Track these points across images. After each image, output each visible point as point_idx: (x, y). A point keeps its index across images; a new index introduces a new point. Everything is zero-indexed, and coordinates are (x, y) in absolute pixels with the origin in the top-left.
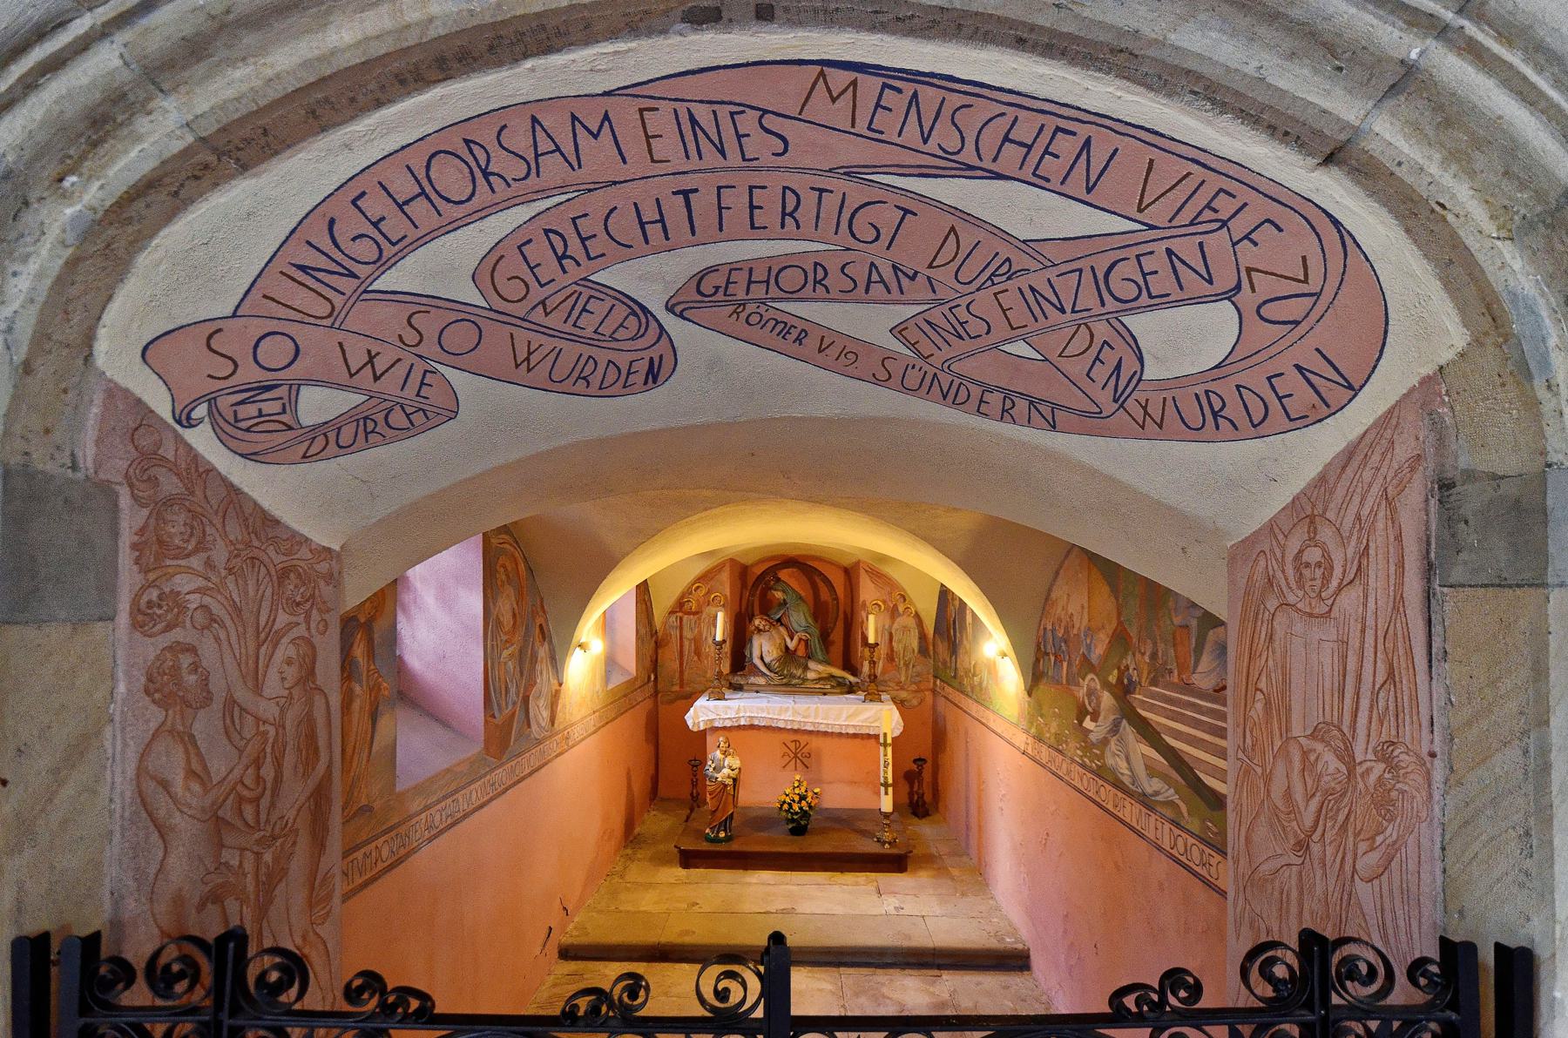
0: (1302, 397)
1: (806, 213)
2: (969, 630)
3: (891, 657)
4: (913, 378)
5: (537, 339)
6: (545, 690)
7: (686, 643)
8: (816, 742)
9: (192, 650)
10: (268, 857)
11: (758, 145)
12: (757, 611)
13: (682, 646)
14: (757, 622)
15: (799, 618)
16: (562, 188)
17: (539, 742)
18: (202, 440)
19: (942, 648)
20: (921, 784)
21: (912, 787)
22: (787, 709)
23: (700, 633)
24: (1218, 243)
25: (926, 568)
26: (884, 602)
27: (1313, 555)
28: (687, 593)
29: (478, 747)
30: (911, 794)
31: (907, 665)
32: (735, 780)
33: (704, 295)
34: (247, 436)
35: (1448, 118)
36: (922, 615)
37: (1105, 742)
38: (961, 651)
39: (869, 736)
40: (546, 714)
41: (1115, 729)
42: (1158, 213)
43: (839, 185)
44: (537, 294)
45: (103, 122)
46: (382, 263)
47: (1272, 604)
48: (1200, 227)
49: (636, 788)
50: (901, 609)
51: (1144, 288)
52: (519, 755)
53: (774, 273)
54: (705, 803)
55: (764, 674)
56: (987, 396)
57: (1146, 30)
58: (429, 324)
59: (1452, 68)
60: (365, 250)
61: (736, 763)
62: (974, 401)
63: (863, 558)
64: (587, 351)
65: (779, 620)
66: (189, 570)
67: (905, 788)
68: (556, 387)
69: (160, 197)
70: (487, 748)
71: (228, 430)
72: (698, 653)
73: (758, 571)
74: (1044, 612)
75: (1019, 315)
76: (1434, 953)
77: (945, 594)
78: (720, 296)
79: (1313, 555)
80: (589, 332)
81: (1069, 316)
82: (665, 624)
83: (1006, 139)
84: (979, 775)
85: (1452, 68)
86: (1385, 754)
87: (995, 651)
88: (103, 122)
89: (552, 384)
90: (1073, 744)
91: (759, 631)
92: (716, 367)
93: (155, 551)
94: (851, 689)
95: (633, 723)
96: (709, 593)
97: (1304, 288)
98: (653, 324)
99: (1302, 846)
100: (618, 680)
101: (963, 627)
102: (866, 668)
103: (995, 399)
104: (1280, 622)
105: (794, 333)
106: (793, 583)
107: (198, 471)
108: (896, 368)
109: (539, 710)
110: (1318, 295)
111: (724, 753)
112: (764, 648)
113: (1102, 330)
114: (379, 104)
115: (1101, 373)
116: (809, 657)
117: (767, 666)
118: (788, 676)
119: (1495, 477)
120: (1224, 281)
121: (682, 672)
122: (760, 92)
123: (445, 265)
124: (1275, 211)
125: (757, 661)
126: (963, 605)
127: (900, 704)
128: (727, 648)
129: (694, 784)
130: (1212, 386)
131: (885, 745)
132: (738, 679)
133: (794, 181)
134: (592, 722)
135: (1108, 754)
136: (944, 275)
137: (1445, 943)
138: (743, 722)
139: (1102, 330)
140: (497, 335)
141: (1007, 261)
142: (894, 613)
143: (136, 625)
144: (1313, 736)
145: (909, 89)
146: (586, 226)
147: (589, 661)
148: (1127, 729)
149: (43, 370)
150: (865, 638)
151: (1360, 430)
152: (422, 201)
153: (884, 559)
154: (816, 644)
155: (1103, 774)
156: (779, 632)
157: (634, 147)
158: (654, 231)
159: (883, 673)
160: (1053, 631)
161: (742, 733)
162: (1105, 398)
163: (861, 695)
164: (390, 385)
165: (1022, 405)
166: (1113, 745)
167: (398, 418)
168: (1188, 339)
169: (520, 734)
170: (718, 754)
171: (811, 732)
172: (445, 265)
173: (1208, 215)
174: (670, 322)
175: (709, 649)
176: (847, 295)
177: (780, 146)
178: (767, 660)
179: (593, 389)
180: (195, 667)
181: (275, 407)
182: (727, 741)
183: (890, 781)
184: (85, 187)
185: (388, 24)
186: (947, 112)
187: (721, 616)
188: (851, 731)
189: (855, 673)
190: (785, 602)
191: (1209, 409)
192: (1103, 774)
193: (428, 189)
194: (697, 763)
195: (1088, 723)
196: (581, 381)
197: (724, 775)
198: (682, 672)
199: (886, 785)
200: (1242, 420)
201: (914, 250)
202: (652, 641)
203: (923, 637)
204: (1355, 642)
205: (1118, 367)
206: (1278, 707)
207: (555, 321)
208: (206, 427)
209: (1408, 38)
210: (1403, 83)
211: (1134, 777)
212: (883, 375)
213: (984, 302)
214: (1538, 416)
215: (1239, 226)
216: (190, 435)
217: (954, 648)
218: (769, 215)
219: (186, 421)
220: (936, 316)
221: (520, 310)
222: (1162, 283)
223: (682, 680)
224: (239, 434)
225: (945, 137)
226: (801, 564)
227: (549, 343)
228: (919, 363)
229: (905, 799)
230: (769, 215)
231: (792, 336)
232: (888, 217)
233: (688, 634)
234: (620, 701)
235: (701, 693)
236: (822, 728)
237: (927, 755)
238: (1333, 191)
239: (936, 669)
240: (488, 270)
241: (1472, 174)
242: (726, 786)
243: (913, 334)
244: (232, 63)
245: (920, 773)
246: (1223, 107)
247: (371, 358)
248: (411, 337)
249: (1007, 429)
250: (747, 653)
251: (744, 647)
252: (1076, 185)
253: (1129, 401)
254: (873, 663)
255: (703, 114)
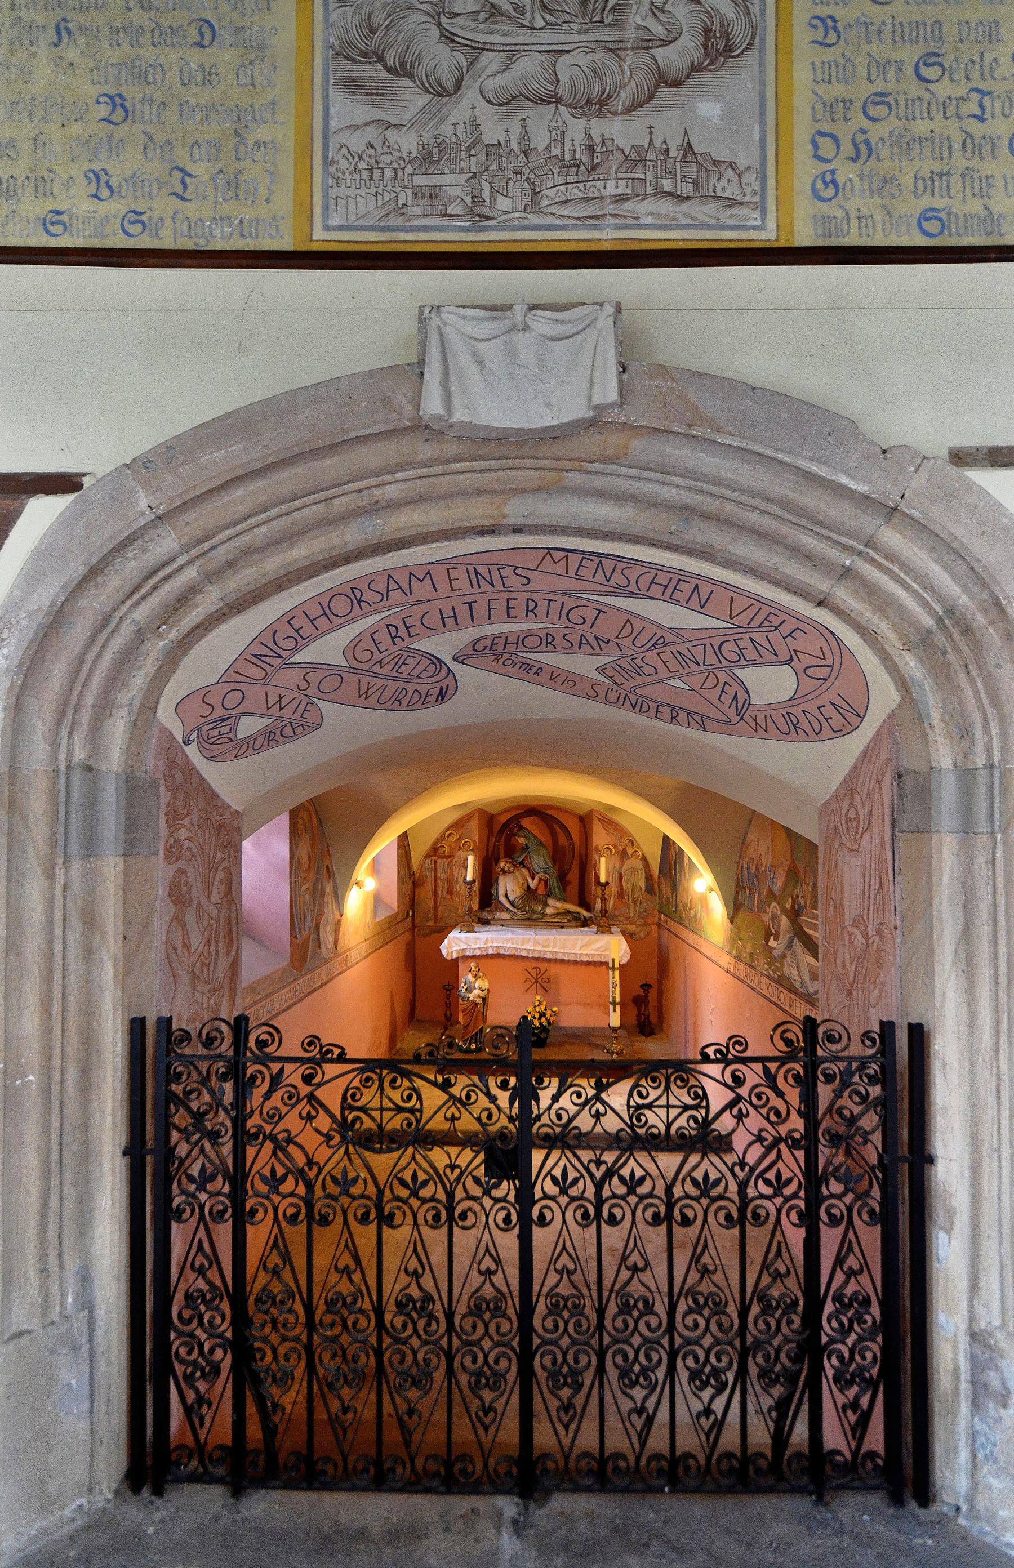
0: (837, 721)
1: (541, 610)
2: (686, 868)
3: (621, 895)
4: (612, 696)
5: (373, 681)
6: (330, 920)
7: (440, 884)
8: (554, 969)
9: (185, 872)
10: (212, 1001)
11: (512, 580)
12: (502, 854)
13: (436, 886)
14: (502, 864)
15: (539, 861)
16: (399, 605)
17: (327, 961)
18: (192, 751)
19: (666, 887)
20: (647, 1006)
21: (639, 1010)
22: (529, 940)
23: (452, 874)
24: (774, 636)
25: (649, 820)
26: (615, 846)
27: (852, 814)
28: (441, 838)
29: (284, 962)
30: (639, 1016)
31: (635, 902)
32: (484, 999)
33: (476, 652)
34: (213, 747)
35: (870, 592)
36: (648, 857)
37: (783, 956)
38: (681, 888)
39: (601, 964)
40: (331, 939)
41: (790, 945)
42: (743, 620)
43: (560, 598)
44: (378, 657)
45: (182, 602)
46: (296, 649)
47: (837, 843)
48: (764, 633)
49: (398, 1009)
50: (630, 852)
51: (741, 655)
52: (314, 970)
53: (521, 639)
54: (458, 1022)
55: (508, 910)
56: (660, 709)
57: (715, 544)
58: (314, 679)
59: (867, 570)
60: (290, 644)
61: (485, 985)
62: (653, 712)
63: (597, 808)
64: (402, 685)
65: (522, 863)
66: (183, 826)
67: (633, 1012)
68: (382, 706)
69: (200, 631)
70: (292, 961)
71: (206, 744)
72: (450, 891)
73: (503, 819)
74: (741, 854)
75: (673, 664)
76: (877, 1029)
77: (666, 839)
78: (487, 651)
79: (852, 814)
80: (404, 675)
81: (702, 667)
82: (421, 866)
83: (652, 582)
84: (695, 995)
85: (867, 570)
86: (879, 933)
87: (703, 885)
88: (182, 602)
89: (380, 705)
90: (762, 961)
91: (504, 872)
92: (483, 693)
93: (174, 816)
94: (585, 923)
95: (396, 949)
96: (460, 838)
97: (823, 662)
98: (444, 668)
99: (850, 993)
100: (383, 914)
101: (682, 867)
102: (598, 905)
103: (666, 711)
104: (840, 853)
105: (534, 670)
106: (533, 829)
107: (189, 769)
108: (602, 692)
109: (327, 936)
110: (832, 666)
111: (475, 976)
112: (509, 887)
113: (722, 676)
114: (312, 577)
115: (727, 699)
116: (549, 894)
117: (512, 903)
118: (530, 913)
119: (917, 773)
120: (784, 656)
121: (436, 909)
122: (517, 560)
123: (329, 648)
124: (800, 625)
125: (502, 899)
126: (681, 851)
127: (629, 936)
128: (476, 887)
129: (448, 1006)
130: (789, 710)
131: (614, 969)
132: (485, 915)
133: (534, 596)
134: (364, 947)
135: (785, 964)
136: (626, 642)
137: (882, 1023)
138: (490, 952)
139: (722, 676)
140: (351, 680)
141: (661, 640)
142: (623, 856)
143: (167, 858)
144: (853, 925)
145: (597, 560)
146: (409, 622)
147: (365, 895)
148: (798, 945)
149: (140, 722)
150: (597, 877)
151: (868, 740)
152: (324, 618)
153: (613, 809)
154: (554, 882)
155: (783, 982)
156: (522, 873)
157: (442, 584)
158: (450, 622)
159: (615, 908)
160: (748, 868)
161: (490, 961)
162: (732, 713)
163: (594, 928)
164: (287, 713)
165: (683, 715)
166: (788, 959)
167: (288, 731)
168: (771, 685)
169: (314, 953)
170: (470, 977)
171: (549, 960)
172: (329, 648)
173: (766, 623)
174: (455, 666)
175: (460, 888)
176: (566, 650)
177: (526, 581)
178: (511, 898)
179: (404, 706)
180: (186, 882)
181: (226, 729)
182: (478, 965)
183: (618, 1000)
184: (169, 632)
185: (324, 546)
186: (618, 570)
187: (471, 859)
188: (585, 959)
189: (589, 908)
190: (527, 847)
191: (790, 723)
192: (783, 982)
193: (328, 612)
194: (451, 988)
195: (772, 943)
196: (397, 702)
197: (474, 995)
198: (436, 909)
199: (614, 1003)
200: (809, 730)
201: (607, 628)
202: (411, 881)
203: (649, 877)
204: (868, 865)
205: (736, 696)
206: (839, 910)
207: (386, 671)
208: (195, 744)
209: (843, 556)
210: (846, 574)
211: (802, 982)
212: (593, 694)
213: (651, 657)
214: (927, 742)
215: (785, 629)
216: (187, 749)
217: (675, 886)
218: (520, 610)
219: (187, 742)
220: (623, 663)
221: (366, 666)
222: (750, 653)
223: (436, 916)
224: (207, 746)
225: (617, 579)
226: (541, 812)
227: (380, 682)
228: (616, 688)
229: (633, 1020)
230: (520, 610)
231: (534, 672)
232: (590, 614)
233: (441, 875)
234: (386, 932)
235: (452, 928)
236: (560, 957)
237: (652, 978)
238: (824, 617)
239: (660, 905)
240: (352, 649)
241: (887, 618)
242: (476, 1004)
243: (610, 672)
244: (244, 568)
245: (646, 996)
246: (762, 579)
247: (280, 698)
248: (303, 685)
249: (674, 728)
250: (494, 892)
251: (491, 886)
252: (694, 602)
253: (743, 715)
254: (604, 899)
255: (483, 570)
